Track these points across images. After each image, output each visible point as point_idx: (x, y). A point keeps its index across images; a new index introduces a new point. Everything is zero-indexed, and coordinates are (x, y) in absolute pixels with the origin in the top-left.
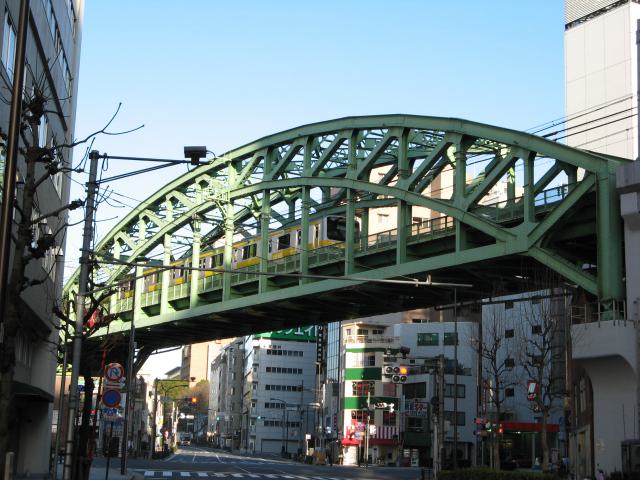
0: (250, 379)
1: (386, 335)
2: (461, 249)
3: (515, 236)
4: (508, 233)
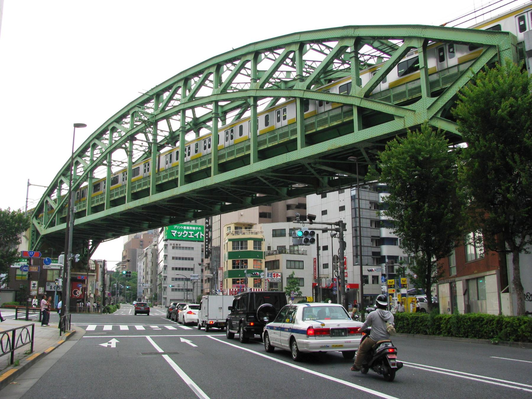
0: (162, 265)
1: (253, 230)
2: (302, 147)
3: (415, 111)
4: (403, 108)
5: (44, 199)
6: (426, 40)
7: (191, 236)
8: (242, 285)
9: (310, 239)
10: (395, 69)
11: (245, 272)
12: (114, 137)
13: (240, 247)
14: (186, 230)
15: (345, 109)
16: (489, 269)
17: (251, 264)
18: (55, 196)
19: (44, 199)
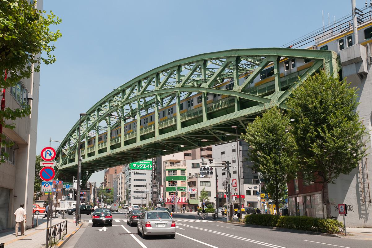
5: (60, 149)
6: (279, 57)
7: (145, 167)
8: (174, 196)
9: (210, 172)
10: (259, 75)
11: (176, 188)
12: (99, 114)
13: (173, 173)
14: (142, 164)
15: (231, 98)
16: (317, 191)
17: (179, 184)
18: (67, 147)
19: (60, 149)
